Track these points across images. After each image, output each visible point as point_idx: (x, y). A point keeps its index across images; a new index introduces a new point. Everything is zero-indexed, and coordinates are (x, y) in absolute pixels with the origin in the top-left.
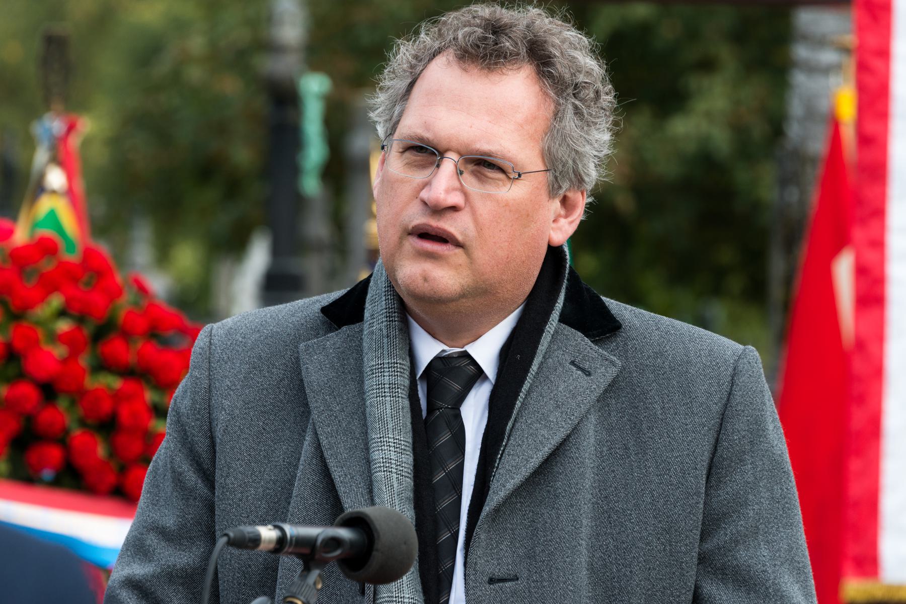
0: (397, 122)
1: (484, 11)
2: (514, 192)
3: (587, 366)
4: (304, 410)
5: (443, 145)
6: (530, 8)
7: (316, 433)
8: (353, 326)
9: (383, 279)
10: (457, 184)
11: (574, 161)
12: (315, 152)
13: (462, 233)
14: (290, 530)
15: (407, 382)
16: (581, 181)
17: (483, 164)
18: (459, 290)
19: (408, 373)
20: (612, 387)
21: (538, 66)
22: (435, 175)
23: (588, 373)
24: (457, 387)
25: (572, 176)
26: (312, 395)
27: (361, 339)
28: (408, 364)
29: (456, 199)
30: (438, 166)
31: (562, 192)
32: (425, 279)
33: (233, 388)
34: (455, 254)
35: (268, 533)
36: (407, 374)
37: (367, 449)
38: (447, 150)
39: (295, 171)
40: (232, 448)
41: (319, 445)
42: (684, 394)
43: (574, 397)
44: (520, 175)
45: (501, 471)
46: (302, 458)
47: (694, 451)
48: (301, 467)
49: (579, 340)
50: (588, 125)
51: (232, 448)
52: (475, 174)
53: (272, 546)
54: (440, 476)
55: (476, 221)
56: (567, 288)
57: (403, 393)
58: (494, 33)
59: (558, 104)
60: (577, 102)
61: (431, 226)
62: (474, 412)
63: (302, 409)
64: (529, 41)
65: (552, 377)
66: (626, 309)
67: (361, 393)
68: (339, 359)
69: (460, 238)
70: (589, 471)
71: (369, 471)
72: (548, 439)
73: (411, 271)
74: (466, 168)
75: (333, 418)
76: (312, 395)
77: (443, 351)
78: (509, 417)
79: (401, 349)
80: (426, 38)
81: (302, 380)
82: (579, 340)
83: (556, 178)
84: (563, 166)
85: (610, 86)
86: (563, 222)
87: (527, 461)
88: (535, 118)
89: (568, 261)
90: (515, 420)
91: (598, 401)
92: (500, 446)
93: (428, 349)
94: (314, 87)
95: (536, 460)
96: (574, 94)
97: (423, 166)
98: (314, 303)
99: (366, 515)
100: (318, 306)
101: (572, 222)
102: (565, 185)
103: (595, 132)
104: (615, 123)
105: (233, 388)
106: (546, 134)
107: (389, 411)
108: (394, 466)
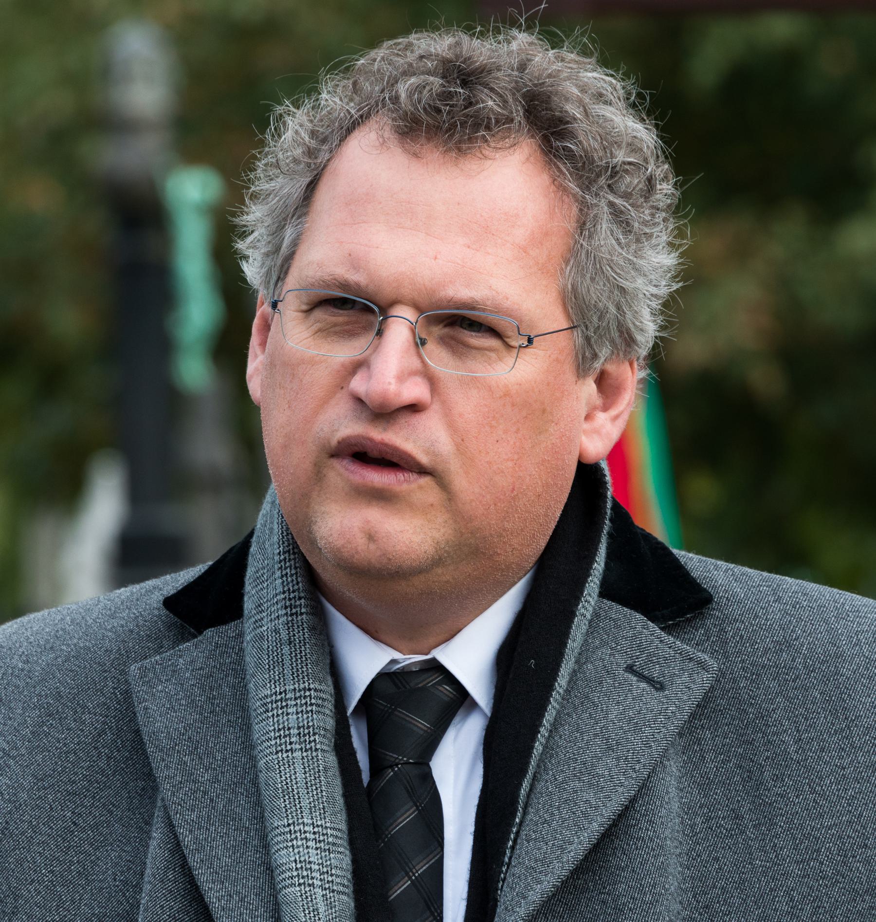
0: (290, 257)
1: (438, 44)
2: (516, 371)
3: (655, 673)
4: (147, 783)
5: (388, 292)
6: (515, 32)
7: (170, 826)
8: (223, 628)
9: (276, 539)
10: (416, 364)
11: (619, 307)
12: (198, 311)
13: (427, 453)
15: (330, 723)
16: (629, 341)
17: (460, 324)
18: (431, 551)
19: (330, 706)
20: (704, 710)
21: (546, 139)
23: (660, 687)
24: (422, 724)
25: (615, 334)
26: (158, 755)
27: (241, 650)
28: (331, 689)
29: (415, 390)
30: (380, 333)
31: (598, 365)
32: (371, 537)
33: (14, 753)
34: (421, 487)
36: (329, 707)
37: (265, 846)
38: (394, 303)
39: (164, 346)
40: (20, 862)
41: (178, 844)
42: (834, 713)
43: (637, 729)
44: (530, 341)
45: (516, 871)
46: (148, 871)
47: (860, 815)
48: (147, 887)
49: (639, 628)
50: (638, 241)
51: (20, 862)
52: (445, 341)
54: (400, 887)
55: (452, 426)
56: (610, 535)
57: (324, 744)
58: (464, 84)
59: (584, 207)
60: (618, 201)
61: (371, 440)
62: (456, 769)
63: (141, 784)
64: (524, 96)
65: (595, 697)
66: (716, 568)
67: (248, 746)
68: (202, 687)
69: (424, 459)
70: (673, 860)
71: (272, 884)
72: (597, 808)
73: (343, 525)
74: (430, 333)
75: (199, 795)
76: (158, 755)
77: (393, 662)
78: (524, 772)
79: (316, 663)
80: (333, 98)
81: (137, 732)
82: (639, 628)
83: (588, 339)
84: (600, 318)
85: (666, 166)
86: (602, 417)
87: (562, 849)
88: (546, 234)
89: (610, 486)
90: (535, 778)
91: (680, 735)
92: (511, 825)
93: (365, 661)
94: (191, 190)
95: (577, 848)
96: (609, 186)
97: (348, 333)
98: (149, 592)
100: (157, 599)
101: (616, 418)
102: (604, 352)
103: (650, 252)
104: (680, 233)
105: (14, 753)
106: (567, 262)
107: (300, 776)
108: (316, 875)
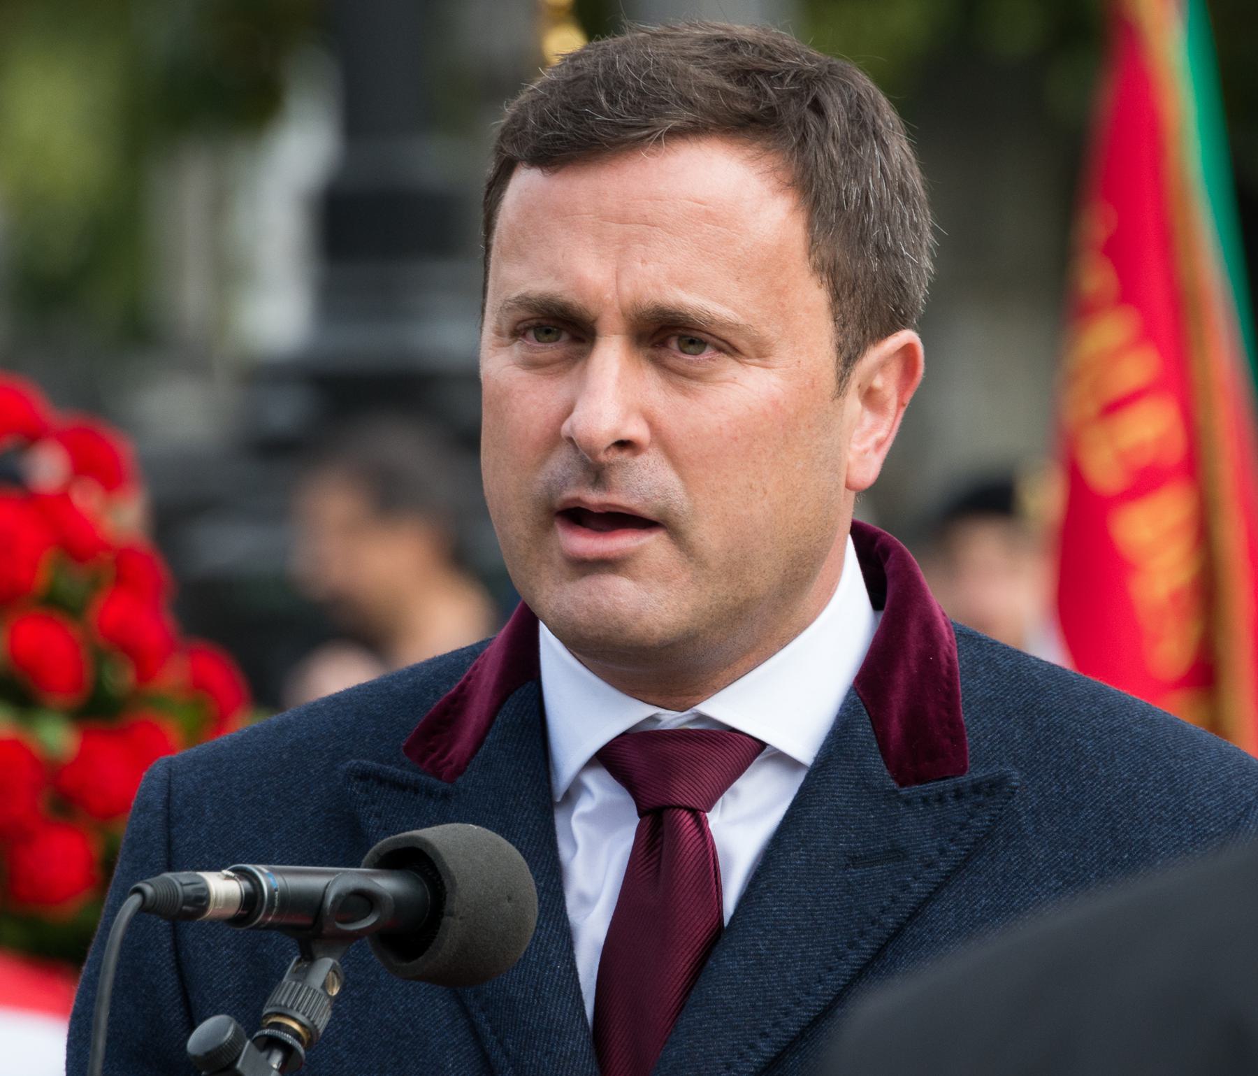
14: (270, 879)
17: (669, 336)
22: (582, 381)
35: (222, 886)
53: (232, 911)
99: (427, 843)
